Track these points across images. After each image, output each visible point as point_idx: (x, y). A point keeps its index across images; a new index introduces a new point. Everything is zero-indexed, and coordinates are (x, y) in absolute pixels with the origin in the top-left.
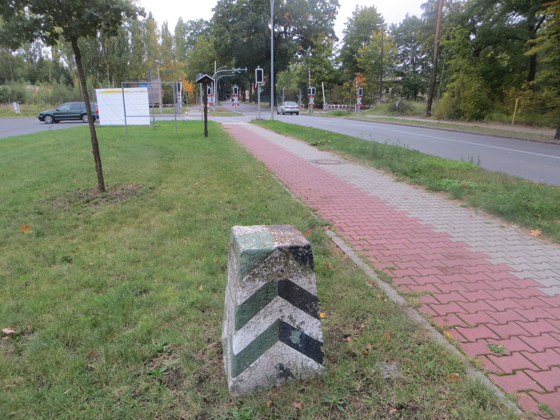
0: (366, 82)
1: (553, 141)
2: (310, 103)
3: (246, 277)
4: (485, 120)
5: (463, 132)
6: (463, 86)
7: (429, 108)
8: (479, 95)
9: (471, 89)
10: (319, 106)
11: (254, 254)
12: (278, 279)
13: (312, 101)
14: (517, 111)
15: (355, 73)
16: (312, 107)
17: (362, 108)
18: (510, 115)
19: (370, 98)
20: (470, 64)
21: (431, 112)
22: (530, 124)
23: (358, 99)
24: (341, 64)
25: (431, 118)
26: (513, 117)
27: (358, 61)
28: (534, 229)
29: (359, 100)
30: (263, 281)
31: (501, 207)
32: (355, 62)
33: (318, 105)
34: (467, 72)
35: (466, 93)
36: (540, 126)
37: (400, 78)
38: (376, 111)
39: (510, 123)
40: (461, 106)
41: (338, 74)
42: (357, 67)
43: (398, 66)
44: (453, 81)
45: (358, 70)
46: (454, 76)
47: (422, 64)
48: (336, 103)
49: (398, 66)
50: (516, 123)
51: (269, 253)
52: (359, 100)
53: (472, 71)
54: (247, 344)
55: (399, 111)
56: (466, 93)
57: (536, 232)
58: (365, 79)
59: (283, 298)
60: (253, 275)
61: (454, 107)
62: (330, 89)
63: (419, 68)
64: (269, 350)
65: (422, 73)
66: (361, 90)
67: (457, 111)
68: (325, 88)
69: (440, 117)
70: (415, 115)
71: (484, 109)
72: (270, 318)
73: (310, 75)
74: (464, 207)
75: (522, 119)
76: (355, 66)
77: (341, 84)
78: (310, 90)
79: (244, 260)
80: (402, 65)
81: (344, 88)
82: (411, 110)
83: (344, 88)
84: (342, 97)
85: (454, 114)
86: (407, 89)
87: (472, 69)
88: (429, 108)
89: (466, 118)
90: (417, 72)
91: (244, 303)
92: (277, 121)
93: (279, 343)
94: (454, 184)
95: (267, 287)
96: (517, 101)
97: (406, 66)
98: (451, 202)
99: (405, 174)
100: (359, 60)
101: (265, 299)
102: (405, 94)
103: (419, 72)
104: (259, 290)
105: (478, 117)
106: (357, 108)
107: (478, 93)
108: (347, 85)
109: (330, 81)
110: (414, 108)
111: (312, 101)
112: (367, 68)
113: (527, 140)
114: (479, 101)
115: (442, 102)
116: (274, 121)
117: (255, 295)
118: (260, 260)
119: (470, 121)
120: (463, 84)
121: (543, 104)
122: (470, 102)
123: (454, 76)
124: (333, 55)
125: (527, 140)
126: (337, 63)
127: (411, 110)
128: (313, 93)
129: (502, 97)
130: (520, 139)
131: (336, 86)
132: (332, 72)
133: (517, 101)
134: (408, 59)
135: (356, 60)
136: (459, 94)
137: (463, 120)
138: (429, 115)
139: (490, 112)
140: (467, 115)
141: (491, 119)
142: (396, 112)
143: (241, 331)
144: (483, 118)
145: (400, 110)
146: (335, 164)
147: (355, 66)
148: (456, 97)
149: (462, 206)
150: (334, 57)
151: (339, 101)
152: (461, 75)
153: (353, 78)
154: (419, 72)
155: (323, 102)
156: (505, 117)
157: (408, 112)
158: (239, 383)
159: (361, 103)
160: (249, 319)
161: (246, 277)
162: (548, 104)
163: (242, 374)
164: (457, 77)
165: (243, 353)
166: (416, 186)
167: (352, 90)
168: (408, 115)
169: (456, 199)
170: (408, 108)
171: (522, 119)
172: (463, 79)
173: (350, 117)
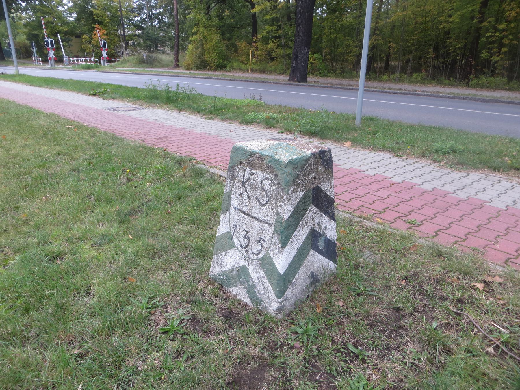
0: (107, 35)
1: (288, 83)
2: (51, 56)
3: (292, 189)
4: (228, 69)
5: (218, 79)
6: (204, 38)
7: (177, 60)
8: (220, 47)
9: (212, 41)
10: (59, 60)
11: (297, 163)
12: (312, 187)
13: (52, 54)
14: (252, 61)
15: (94, 25)
16: (53, 61)
17: (109, 61)
18: (246, 64)
19: (113, 51)
20: (207, 19)
21: (180, 64)
22: (263, 71)
23: (103, 52)
24: (75, 15)
25: (181, 68)
26: (250, 66)
27: (94, 13)
28: (346, 142)
29: (104, 53)
30: (303, 191)
31: (313, 129)
32: (91, 14)
33: (58, 59)
34: (205, 26)
35: (208, 46)
36: (271, 72)
37: (140, 32)
38: (125, 63)
39: (247, 71)
40: (206, 57)
41: (74, 25)
42: (94, 19)
43: (136, 19)
44: (196, 33)
45: (95, 22)
46: (195, 30)
47: (158, 19)
48: (77, 57)
49: (136, 19)
50: (253, 71)
51: (307, 160)
52: (104, 53)
53: (210, 25)
54: (291, 260)
55: (147, 63)
56: (208, 46)
57: (348, 144)
58: (104, 31)
59: (315, 206)
60: (296, 185)
61: (199, 58)
62: (68, 42)
63: (156, 23)
64: (305, 261)
65: (159, 28)
66: (104, 43)
67: (202, 62)
68: (63, 41)
69: (188, 68)
70: (163, 66)
71: (225, 60)
72: (306, 228)
73: (44, 26)
74: (282, 133)
75: (255, 67)
76: (91, 18)
77: (78, 36)
78: (47, 42)
79: (289, 170)
80: (139, 19)
81: (83, 40)
82: (159, 62)
83: (83, 40)
84: (83, 50)
85: (200, 65)
86: (149, 42)
87: (210, 24)
88: (177, 60)
89: (211, 68)
90: (155, 26)
91: (289, 217)
92: (23, 75)
93: (312, 252)
94: (260, 117)
95: (305, 197)
96: (251, 52)
97: (143, 20)
98: (268, 131)
99: (211, 112)
100: (95, 11)
101: (303, 209)
102: (147, 47)
103: (157, 26)
104: (300, 201)
105: (221, 67)
106: (104, 61)
107: (219, 45)
108: (86, 37)
109: (66, 33)
110: (161, 60)
111: (52, 54)
112: (105, 20)
113: (270, 83)
114: (220, 52)
115: (190, 52)
116: (20, 75)
117: (297, 207)
118: (301, 168)
119: (215, 70)
120: (205, 37)
121: (269, 54)
122: (213, 53)
123: (195, 30)
124: (65, 4)
125: (270, 83)
126: (70, 14)
127: (159, 62)
128: (52, 45)
129: (237, 49)
130: (265, 82)
131: (74, 39)
132: (65, 23)
133: (251, 52)
134: (144, 13)
135: (92, 12)
136: (202, 45)
137: (209, 70)
138: (178, 66)
139: (230, 62)
140: (213, 65)
141: (232, 68)
142: (145, 64)
143: (287, 248)
144: (226, 67)
145: (149, 62)
146: (134, 110)
147: (91, 18)
148: (200, 49)
149: (280, 133)
150: (66, 7)
151: (80, 55)
152: (201, 29)
153: (91, 30)
154: (157, 26)
155: (63, 56)
156: (243, 66)
157: (157, 64)
158: (284, 302)
159: (106, 56)
160: (293, 233)
161: (292, 189)
162: (273, 54)
163: (287, 293)
164: (198, 31)
165: (288, 271)
166: (229, 122)
167: (93, 42)
168: (156, 67)
169: (271, 128)
170: (155, 60)
171: (255, 67)
172: (203, 32)
173: (101, 70)
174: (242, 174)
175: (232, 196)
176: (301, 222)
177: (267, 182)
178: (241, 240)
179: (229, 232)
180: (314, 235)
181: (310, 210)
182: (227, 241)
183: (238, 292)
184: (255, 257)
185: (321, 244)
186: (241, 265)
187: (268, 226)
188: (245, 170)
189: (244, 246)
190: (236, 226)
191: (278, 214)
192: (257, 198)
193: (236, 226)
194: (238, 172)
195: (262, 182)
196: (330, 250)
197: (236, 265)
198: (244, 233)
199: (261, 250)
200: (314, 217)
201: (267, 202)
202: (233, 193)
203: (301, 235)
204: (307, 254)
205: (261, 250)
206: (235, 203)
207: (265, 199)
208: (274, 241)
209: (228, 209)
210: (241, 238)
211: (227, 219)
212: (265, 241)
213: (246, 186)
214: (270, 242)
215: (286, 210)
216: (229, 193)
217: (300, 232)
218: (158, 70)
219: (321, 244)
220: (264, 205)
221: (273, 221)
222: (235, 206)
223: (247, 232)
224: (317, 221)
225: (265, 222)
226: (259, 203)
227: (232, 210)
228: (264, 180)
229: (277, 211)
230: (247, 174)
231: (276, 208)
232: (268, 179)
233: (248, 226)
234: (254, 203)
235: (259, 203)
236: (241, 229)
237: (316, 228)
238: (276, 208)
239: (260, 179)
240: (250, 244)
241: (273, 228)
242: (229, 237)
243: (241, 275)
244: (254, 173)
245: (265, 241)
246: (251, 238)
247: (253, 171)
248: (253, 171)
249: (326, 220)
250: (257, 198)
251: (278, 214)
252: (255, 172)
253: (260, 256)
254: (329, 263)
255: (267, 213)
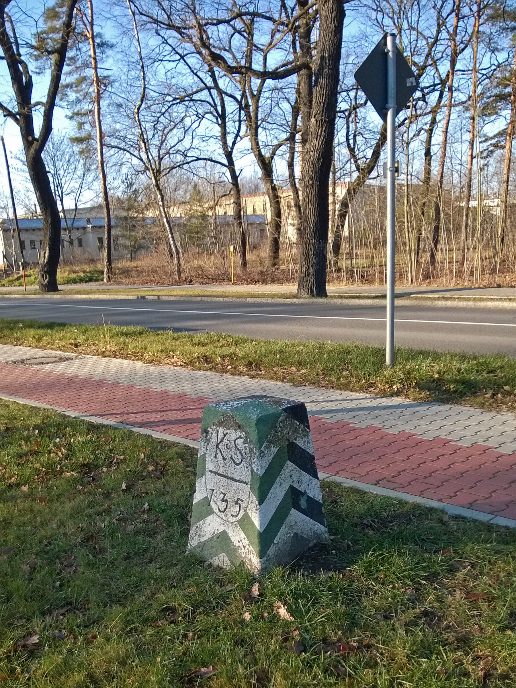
72: (284, 485)
174: (215, 435)
175: (207, 459)
176: (278, 479)
177: (240, 441)
178: (219, 504)
179: (207, 497)
180: (294, 496)
181: (287, 467)
182: (206, 508)
183: (222, 560)
184: (235, 519)
185: (303, 503)
186: (221, 531)
187: (245, 485)
188: (218, 431)
189: (223, 510)
190: (213, 490)
191: (253, 471)
192: (231, 458)
193: (213, 490)
194: (212, 433)
195: (235, 441)
196: (313, 509)
197: (216, 532)
198: (222, 495)
199: (239, 511)
200: (291, 474)
201: (242, 461)
202: (207, 455)
203: (278, 493)
204: (287, 514)
205: (239, 511)
206: (210, 466)
207: (240, 457)
208: (251, 499)
209: (203, 474)
210: (219, 502)
211: (203, 484)
212: (242, 501)
213: (220, 446)
214: (247, 500)
215: (259, 467)
216: (204, 455)
217: (278, 489)
218: (87, 296)
219: (303, 503)
220: (238, 464)
221: (248, 479)
222: (211, 469)
223: (225, 494)
224: (295, 478)
225: (241, 482)
226: (234, 462)
227: (208, 474)
228: (237, 439)
229: (252, 468)
230: (221, 435)
231: (251, 465)
232: (242, 438)
233: (225, 487)
234: (229, 463)
235: (234, 462)
236: (219, 492)
237: (296, 486)
238: (251, 465)
239: (233, 439)
240: (228, 507)
241: (249, 486)
242: (206, 502)
243: (223, 538)
244: (227, 433)
245: (242, 501)
246: (229, 500)
247: (226, 431)
248: (226, 431)
249: (306, 476)
250: (231, 458)
251: (253, 471)
252: (228, 431)
253: (239, 517)
254: (315, 525)
255: (243, 473)
